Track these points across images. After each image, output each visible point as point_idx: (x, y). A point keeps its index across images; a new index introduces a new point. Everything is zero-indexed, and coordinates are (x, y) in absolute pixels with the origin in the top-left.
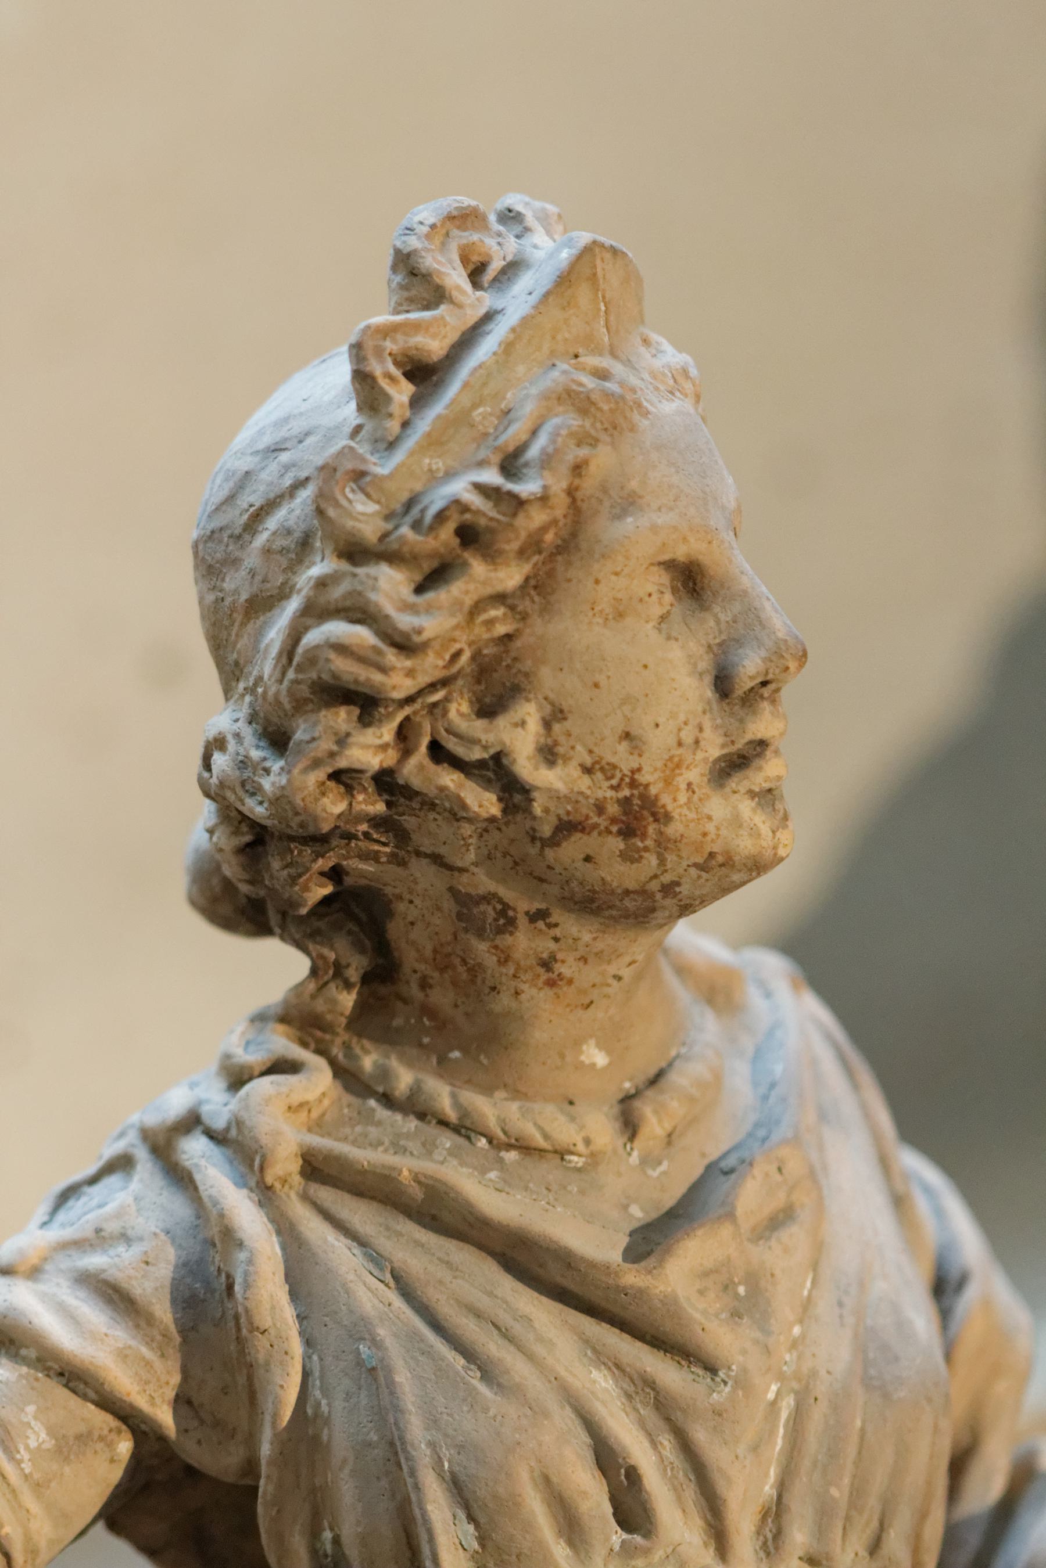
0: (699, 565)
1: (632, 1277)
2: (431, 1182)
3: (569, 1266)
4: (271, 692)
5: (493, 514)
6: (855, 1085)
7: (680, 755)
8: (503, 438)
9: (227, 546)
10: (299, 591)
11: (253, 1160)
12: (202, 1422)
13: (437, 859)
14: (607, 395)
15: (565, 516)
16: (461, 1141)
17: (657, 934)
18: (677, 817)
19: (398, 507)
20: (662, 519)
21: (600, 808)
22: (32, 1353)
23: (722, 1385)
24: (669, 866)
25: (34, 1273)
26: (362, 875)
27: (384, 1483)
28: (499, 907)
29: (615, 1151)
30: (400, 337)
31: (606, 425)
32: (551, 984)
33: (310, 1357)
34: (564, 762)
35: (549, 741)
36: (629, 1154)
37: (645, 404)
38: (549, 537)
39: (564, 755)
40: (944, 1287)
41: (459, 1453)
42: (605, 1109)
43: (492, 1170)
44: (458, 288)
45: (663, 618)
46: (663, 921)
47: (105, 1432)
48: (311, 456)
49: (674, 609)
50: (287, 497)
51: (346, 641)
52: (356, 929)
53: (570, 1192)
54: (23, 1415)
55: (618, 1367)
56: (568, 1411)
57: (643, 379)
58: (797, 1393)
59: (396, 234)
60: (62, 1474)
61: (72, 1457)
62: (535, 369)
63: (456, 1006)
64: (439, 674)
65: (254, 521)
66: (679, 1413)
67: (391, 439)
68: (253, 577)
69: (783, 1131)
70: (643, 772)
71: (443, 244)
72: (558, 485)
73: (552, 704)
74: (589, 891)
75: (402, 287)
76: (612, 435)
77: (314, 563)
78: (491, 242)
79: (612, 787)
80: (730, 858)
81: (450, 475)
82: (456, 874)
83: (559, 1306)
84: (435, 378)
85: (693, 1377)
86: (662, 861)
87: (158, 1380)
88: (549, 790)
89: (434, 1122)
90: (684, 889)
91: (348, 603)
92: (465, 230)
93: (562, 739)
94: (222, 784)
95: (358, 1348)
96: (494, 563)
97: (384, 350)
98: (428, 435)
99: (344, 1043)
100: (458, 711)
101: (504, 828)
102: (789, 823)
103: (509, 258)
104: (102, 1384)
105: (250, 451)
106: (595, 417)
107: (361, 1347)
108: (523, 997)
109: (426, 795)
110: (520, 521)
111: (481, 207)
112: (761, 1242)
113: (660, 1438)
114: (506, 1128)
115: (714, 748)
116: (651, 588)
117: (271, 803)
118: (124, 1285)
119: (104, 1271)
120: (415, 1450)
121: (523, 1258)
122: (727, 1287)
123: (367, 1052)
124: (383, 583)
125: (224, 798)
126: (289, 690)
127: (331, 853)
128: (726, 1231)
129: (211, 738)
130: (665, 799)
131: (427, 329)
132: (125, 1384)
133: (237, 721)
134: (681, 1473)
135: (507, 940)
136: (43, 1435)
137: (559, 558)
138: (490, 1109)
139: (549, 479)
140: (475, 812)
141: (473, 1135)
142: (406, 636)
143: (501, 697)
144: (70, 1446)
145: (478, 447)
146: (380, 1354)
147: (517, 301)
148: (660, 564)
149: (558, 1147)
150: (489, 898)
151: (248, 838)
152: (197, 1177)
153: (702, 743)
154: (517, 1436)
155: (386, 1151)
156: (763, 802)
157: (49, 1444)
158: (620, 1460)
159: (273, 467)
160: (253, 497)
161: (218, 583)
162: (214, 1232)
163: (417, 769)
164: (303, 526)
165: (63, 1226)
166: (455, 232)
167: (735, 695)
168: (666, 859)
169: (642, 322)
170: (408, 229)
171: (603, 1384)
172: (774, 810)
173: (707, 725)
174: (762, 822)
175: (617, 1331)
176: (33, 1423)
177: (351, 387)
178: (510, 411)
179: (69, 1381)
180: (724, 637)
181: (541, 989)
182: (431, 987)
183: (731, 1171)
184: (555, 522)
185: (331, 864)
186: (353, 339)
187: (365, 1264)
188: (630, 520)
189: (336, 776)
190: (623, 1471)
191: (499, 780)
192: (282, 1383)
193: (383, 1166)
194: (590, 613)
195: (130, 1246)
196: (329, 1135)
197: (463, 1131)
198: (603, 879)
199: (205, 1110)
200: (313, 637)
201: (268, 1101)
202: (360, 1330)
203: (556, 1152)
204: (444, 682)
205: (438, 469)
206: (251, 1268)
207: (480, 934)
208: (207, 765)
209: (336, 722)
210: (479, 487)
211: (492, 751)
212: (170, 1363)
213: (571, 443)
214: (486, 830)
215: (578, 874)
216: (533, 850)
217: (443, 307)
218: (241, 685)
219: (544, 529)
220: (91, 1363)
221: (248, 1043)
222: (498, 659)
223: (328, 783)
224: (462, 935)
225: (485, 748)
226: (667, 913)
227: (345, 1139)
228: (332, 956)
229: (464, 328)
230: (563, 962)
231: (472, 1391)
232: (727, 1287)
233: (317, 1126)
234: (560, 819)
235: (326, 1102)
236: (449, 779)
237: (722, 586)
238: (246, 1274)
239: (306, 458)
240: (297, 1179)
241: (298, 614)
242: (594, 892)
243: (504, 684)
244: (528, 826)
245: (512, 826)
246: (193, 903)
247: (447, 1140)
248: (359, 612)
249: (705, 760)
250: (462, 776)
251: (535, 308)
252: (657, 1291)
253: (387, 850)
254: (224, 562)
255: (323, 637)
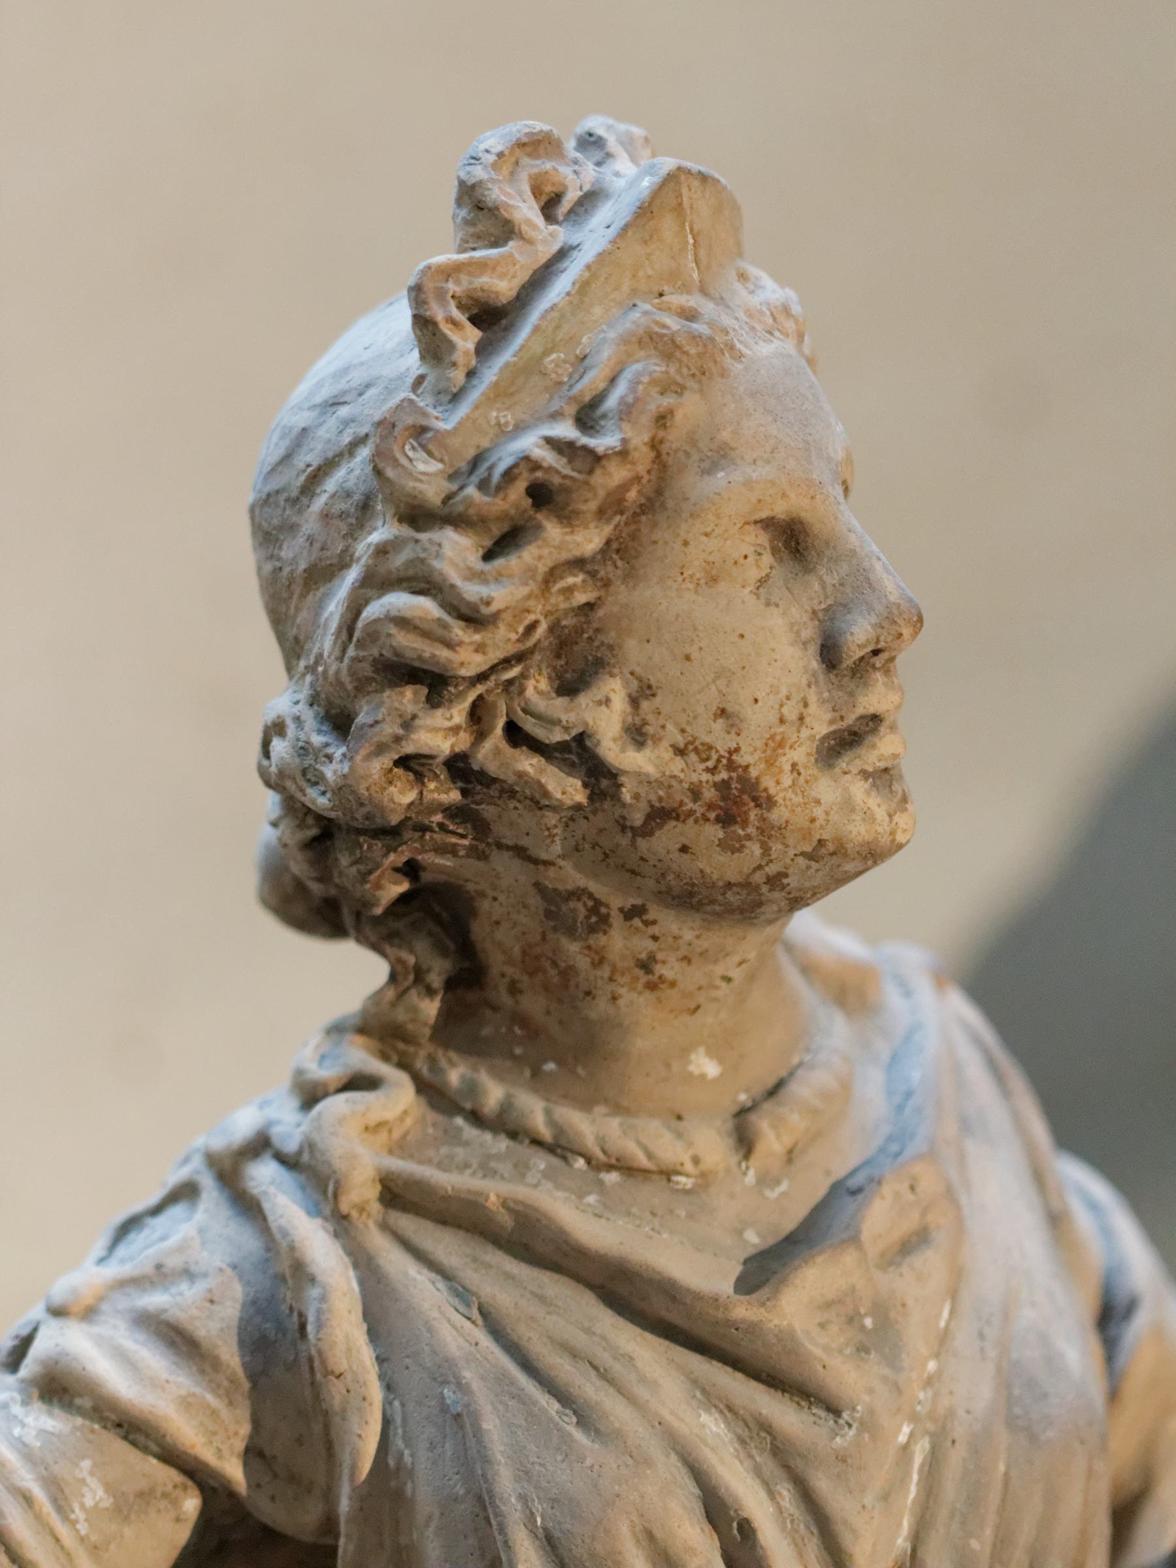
0: (801, 523)
1: (744, 1310)
2: (521, 1208)
3: (673, 1299)
4: (332, 671)
5: (567, 471)
6: (1006, 1092)
7: (783, 733)
8: (578, 387)
9: (285, 509)
10: (359, 559)
11: (326, 1186)
12: (275, 1476)
13: (521, 852)
14: (694, 337)
15: (649, 472)
16: (555, 1161)
17: (770, 930)
18: (781, 801)
19: (463, 465)
20: (760, 473)
21: (695, 793)
22: (86, 1402)
23: (846, 1428)
24: (773, 857)
25: (89, 1314)
26: (441, 869)
27: (472, 1541)
28: (590, 903)
29: (728, 1171)
30: (464, 279)
31: (693, 370)
32: (652, 987)
33: (391, 1403)
34: (654, 743)
35: (637, 720)
36: (745, 1174)
37: (738, 345)
38: (632, 495)
39: (654, 736)
40: (1111, 1315)
41: (552, 1508)
42: (718, 1123)
43: (590, 1193)
44: (529, 222)
45: (762, 582)
46: (774, 916)
47: (170, 1487)
48: (371, 409)
49: (774, 572)
50: (347, 456)
51: (408, 614)
52: (437, 929)
53: (678, 1216)
54: (77, 1471)
55: (729, 1410)
56: (674, 1458)
57: (737, 319)
58: (932, 1435)
59: (461, 164)
60: (122, 1536)
61: (133, 1517)
62: (614, 310)
63: (548, 1013)
64: (511, 649)
65: (312, 483)
66: (798, 1460)
67: (455, 390)
68: (311, 544)
69: (917, 1145)
70: (742, 752)
71: (512, 173)
72: (639, 439)
73: (640, 679)
74: (686, 884)
75: (467, 222)
76: (700, 382)
77: (375, 529)
78: (566, 171)
79: (707, 770)
80: (842, 846)
81: (520, 428)
82: (541, 868)
83: (666, 1343)
84: (504, 322)
85: (813, 1419)
86: (766, 850)
87: (226, 1430)
88: (639, 774)
89: (527, 1141)
90: (792, 881)
91: (411, 572)
92: (538, 157)
93: (651, 718)
94: (281, 774)
95: (442, 1393)
96: (570, 525)
97: (447, 292)
98: (496, 384)
99: (429, 1055)
100: (535, 688)
101: (591, 817)
102: (909, 806)
103: (586, 188)
104: (164, 1436)
105: (307, 405)
106: (680, 361)
107: (446, 1391)
108: (621, 1002)
109: (505, 781)
110: (598, 479)
111: (555, 132)
112: (891, 1269)
113: (779, 1487)
114: (606, 1148)
115: (821, 725)
116: (748, 549)
117: (334, 793)
118: (188, 1327)
119: (165, 1311)
120: (504, 1504)
121: (623, 1290)
122: (853, 1319)
123: (453, 1064)
124: (447, 550)
125: (284, 788)
126: (350, 668)
127: (404, 847)
128: (850, 1258)
129: (269, 724)
130: (768, 782)
131: (494, 269)
132: (189, 1434)
133: (297, 703)
134: (802, 1526)
135: (599, 940)
136: (100, 1493)
137: (644, 518)
138: (588, 1127)
139: (628, 431)
140: (557, 800)
141: (569, 1155)
142: (474, 608)
143: (583, 673)
144: (130, 1504)
145: (551, 398)
146: (466, 1398)
147: (594, 235)
148: (756, 522)
149: (664, 1168)
150: (577, 894)
151: (314, 832)
152: (266, 1206)
153: (808, 720)
154: (617, 1487)
155: (474, 1174)
156: (878, 782)
157: (108, 1502)
158: (732, 1513)
159: (332, 423)
160: (310, 457)
161: (276, 551)
162: (285, 1266)
163: (493, 753)
164: (363, 488)
165: (122, 1261)
166: (525, 160)
167: (844, 665)
168: (771, 848)
169: (740, 254)
170: (473, 158)
171: (714, 1429)
172: (891, 791)
173: (813, 698)
174: (877, 806)
175: (730, 1370)
176: (89, 1480)
177: (412, 336)
178: (585, 357)
179: (128, 1432)
180: (829, 602)
181: (640, 993)
182: (521, 992)
183: (859, 1191)
184: (638, 479)
185: (404, 859)
186: (412, 281)
187: (451, 1300)
188: (721, 474)
189: (404, 762)
190: (735, 1525)
191: (582, 763)
192: (359, 1432)
193: (469, 1192)
194: (680, 579)
195: (193, 1283)
196: (411, 1157)
197: (559, 1151)
198: (702, 871)
199: (276, 1132)
200: (374, 610)
201: (341, 1121)
202: (444, 1373)
203: (661, 1172)
204: (520, 657)
205: (507, 423)
206: (324, 1306)
207: (571, 932)
208: (266, 752)
209: (401, 703)
210: (550, 442)
211: (574, 732)
212: (238, 1411)
213: (654, 391)
214: (572, 819)
215: (674, 866)
216: (624, 841)
217: (511, 243)
218: (302, 663)
219: (624, 487)
220: (151, 1413)
221: (323, 1058)
222: (579, 630)
223: (396, 770)
224: (551, 936)
225: (566, 729)
226: (775, 908)
227: (429, 1162)
228: (411, 960)
229: (536, 266)
230: (664, 962)
231: (566, 1438)
232: (853, 1319)
233: (399, 1148)
234: (652, 806)
235: (409, 1121)
236: (528, 764)
237: (827, 543)
238: (319, 1312)
239: (366, 412)
240: (375, 1207)
241: (357, 585)
242: (693, 885)
243: (586, 657)
244: (616, 814)
245: (600, 816)
246: (265, 902)
247: (541, 1161)
248: (423, 582)
249: (812, 738)
250: (543, 760)
251: (613, 242)
252: (771, 1325)
253: (466, 842)
254: (280, 528)
255: (384, 610)
